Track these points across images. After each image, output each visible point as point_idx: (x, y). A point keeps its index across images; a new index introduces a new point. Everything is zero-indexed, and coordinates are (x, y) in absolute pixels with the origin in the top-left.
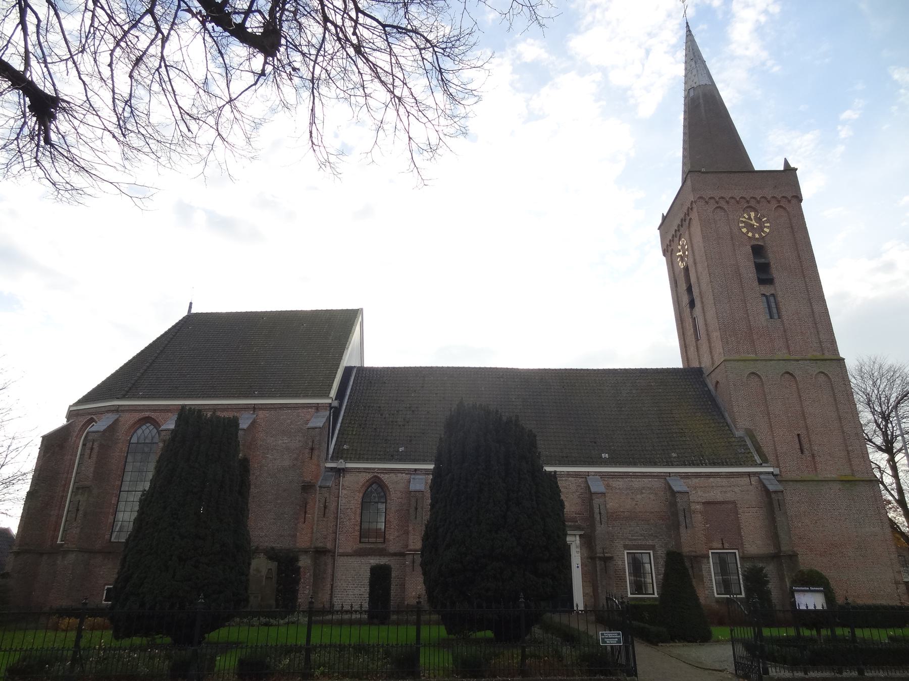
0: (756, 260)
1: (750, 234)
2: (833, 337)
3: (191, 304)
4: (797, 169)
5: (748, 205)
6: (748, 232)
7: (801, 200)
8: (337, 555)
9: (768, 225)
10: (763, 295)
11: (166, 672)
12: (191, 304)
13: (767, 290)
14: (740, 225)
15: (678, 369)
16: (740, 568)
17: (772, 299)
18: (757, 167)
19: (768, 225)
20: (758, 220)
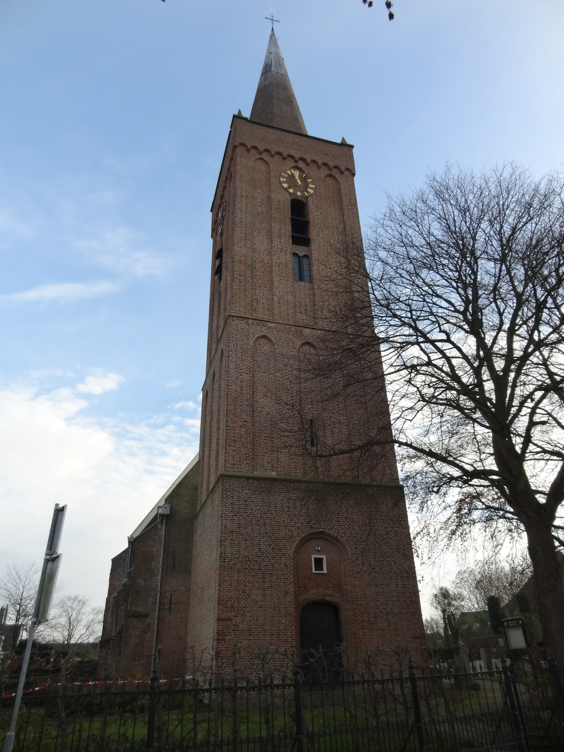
0: (294, 235)
1: (291, 191)
2: (373, 356)
3: (59, 512)
4: (352, 147)
5: (296, 165)
6: (289, 187)
7: (354, 175)
8: (28, 700)
9: (313, 186)
10: (295, 254)
11: (208, 664)
12: (59, 512)
13: (301, 251)
14: (281, 179)
15: (421, 615)
16: (510, 420)
17: (305, 261)
18: (311, 131)
19: (313, 186)
20: (304, 180)
